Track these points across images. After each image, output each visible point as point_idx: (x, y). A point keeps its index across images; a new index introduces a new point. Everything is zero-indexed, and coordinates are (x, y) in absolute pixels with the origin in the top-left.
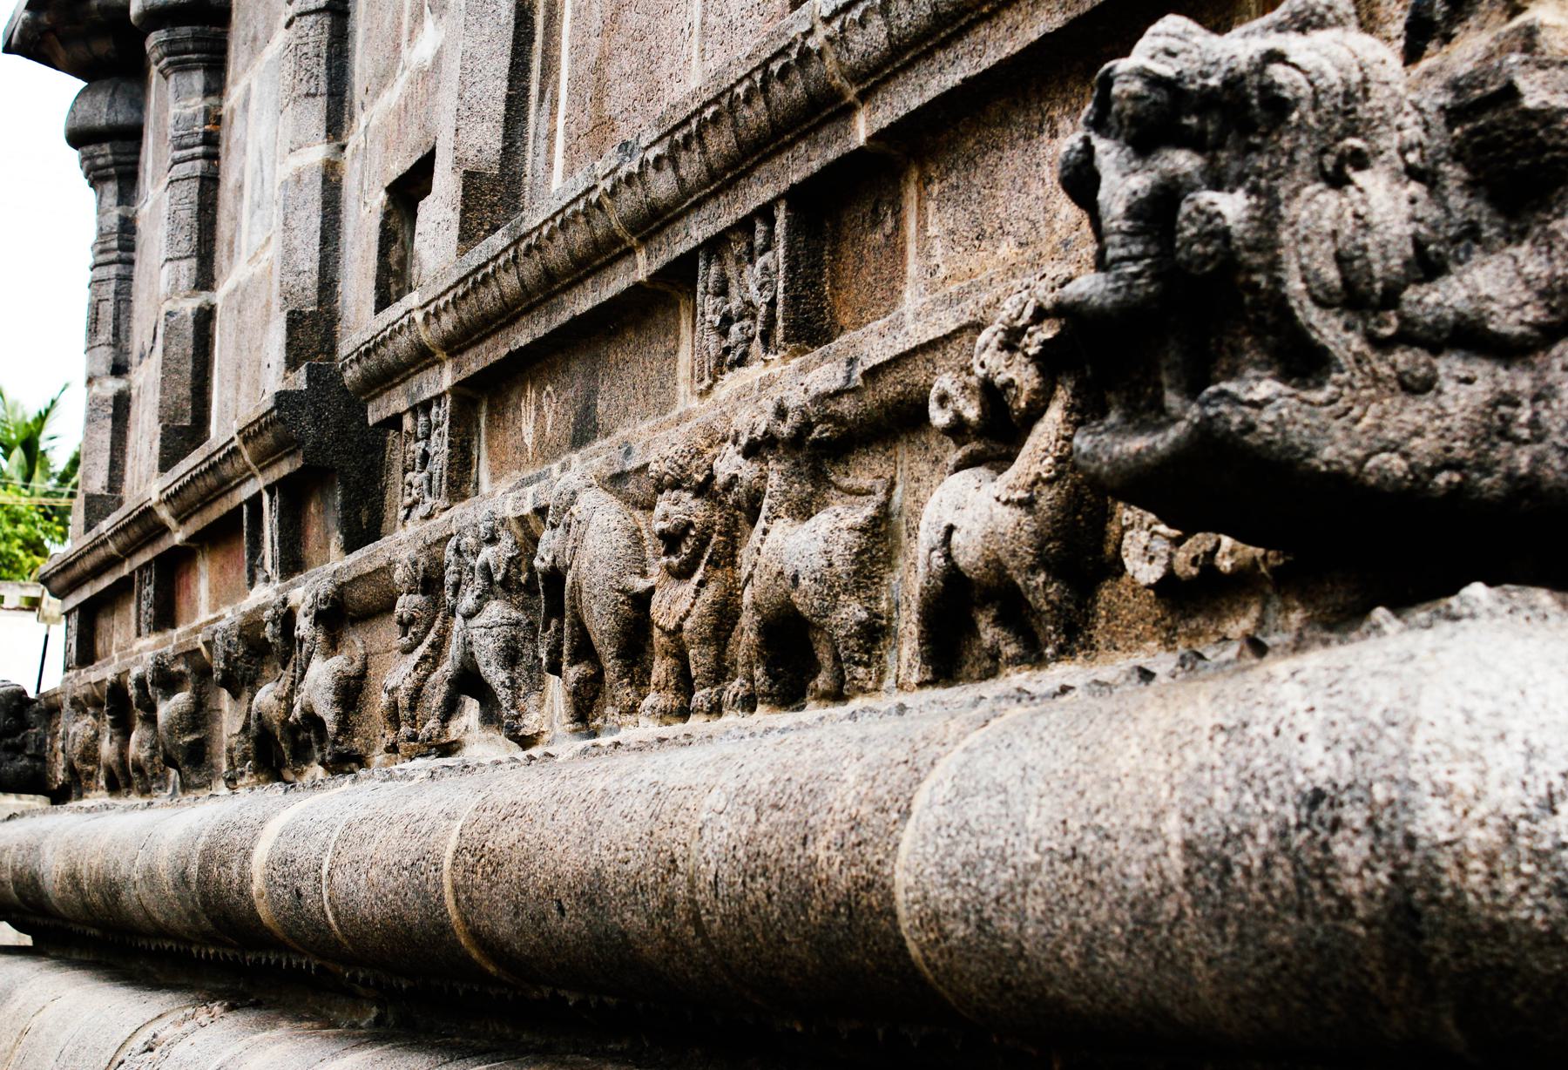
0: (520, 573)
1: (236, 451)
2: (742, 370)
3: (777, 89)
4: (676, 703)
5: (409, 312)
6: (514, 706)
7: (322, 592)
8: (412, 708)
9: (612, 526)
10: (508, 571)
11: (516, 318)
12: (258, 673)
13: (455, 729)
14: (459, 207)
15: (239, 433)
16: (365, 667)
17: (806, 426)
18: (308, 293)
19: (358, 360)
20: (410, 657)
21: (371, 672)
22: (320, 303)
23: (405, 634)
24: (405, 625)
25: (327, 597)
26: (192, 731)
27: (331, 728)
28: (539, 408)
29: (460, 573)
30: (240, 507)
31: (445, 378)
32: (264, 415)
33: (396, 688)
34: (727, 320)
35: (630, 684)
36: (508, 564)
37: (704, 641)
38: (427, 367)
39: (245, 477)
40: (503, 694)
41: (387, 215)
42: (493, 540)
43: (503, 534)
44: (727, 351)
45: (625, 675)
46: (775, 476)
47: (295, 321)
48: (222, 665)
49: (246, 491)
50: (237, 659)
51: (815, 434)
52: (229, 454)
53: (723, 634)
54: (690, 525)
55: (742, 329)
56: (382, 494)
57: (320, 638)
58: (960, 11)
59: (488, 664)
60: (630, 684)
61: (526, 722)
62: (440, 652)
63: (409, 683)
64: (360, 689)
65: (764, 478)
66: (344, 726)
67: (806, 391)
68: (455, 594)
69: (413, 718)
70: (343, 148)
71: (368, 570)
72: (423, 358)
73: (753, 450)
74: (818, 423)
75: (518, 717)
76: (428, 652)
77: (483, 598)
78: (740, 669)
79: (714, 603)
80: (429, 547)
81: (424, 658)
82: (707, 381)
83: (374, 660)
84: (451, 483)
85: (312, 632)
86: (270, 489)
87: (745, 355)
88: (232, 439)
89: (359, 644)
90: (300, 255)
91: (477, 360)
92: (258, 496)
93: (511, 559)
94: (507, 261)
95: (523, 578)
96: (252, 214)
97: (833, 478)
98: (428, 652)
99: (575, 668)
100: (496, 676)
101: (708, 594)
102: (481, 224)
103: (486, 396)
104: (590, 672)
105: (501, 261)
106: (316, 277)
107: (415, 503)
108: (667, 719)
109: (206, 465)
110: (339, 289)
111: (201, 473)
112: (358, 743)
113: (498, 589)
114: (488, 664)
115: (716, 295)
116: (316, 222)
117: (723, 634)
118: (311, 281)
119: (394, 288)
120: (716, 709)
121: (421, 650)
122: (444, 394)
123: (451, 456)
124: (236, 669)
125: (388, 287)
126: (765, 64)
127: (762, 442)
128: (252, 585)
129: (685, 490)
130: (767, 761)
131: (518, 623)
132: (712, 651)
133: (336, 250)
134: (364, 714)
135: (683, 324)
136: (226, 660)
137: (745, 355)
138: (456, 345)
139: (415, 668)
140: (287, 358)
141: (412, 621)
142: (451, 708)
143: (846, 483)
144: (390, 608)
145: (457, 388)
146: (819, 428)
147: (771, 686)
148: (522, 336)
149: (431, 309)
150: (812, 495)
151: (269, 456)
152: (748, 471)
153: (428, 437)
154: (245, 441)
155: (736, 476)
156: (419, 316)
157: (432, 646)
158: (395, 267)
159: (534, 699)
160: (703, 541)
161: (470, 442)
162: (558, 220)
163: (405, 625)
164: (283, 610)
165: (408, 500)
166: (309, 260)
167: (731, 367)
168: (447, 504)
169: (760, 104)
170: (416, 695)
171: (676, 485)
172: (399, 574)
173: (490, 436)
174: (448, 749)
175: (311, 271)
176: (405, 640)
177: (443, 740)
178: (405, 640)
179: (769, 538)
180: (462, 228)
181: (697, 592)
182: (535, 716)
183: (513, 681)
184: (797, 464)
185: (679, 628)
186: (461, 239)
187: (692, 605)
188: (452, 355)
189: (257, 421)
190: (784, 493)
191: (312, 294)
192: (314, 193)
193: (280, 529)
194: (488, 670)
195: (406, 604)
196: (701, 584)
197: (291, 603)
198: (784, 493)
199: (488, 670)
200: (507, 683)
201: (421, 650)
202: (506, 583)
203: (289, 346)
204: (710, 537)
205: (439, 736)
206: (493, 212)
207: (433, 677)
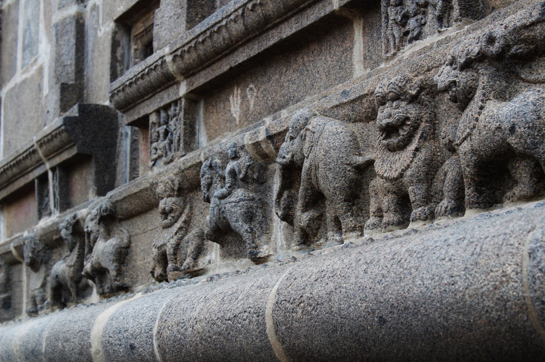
0: (254, 173)
1: (34, 152)
2: (418, 42)
3: (187, 56)
4: (396, 219)
5: (162, 57)
6: (253, 242)
7: (104, 206)
8: (175, 254)
9: (339, 131)
10: (247, 172)
11: (236, 49)
12: (50, 258)
13: (202, 262)
14: (186, 6)
15: (37, 142)
16: (130, 242)
17: (506, 47)
18: (70, 75)
19: (123, 90)
20: (170, 229)
21: (133, 245)
22: (76, 80)
23: (166, 218)
24: (165, 214)
25: (107, 208)
26: (5, 292)
27: (113, 273)
28: (244, 97)
29: (212, 178)
30: (33, 182)
31: (183, 89)
32: (55, 130)
33: (164, 245)
34: (406, 17)
35: (352, 215)
36: (247, 169)
37: (419, 181)
38: (171, 85)
39: (40, 163)
40: (246, 236)
41: (115, 33)
42: (235, 157)
43: (242, 153)
44: (406, 33)
45: (349, 211)
46: (483, 78)
47: (64, 88)
48: (30, 255)
49: (38, 172)
50: (39, 251)
51: (513, 50)
52: (30, 154)
53: (430, 177)
54: (408, 119)
55: (417, 20)
56: (115, 168)
57: (102, 230)
58: (297, 5)
59: (237, 221)
60: (352, 215)
61: (261, 250)
62: (189, 225)
63: (173, 241)
64: (127, 254)
65: (477, 80)
66: (120, 273)
67: (506, 27)
68: (208, 190)
69: (176, 259)
70: (85, 7)
71: (136, 191)
72: (167, 81)
73: (467, 65)
74: (514, 45)
75: (256, 247)
76: (183, 225)
77: (233, 187)
78: (446, 194)
79: (425, 159)
80: (183, 171)
81: (180, 228)
82: (393, 51)
83: (133, 240)
84: (186, 143)
85: (97, 228)
86: (53, 169)
87: (420, 34)
88: (33, 146)
89: (125, 231)
90: (65, 57)
91: (201, 79)
92: (45, 174)
93: (249, 166)
94: (237, 16)
95: (255, 176)
96: (24, 50)
97: (523, 76)
98: (183, 225)
99: (306, 214)
100: (242, 227)
101: (422, 155)
102: (197, 14)
103: (210, 94)
104: (316, 214)
105: (232, 17)
106: (73, 68)
107: (160, 157)
108: (390, 227)
109: (15, 162)
110: (85, 73)
111: (11, 167)
112: (127, 281)
113: (241, 183)
114: (237, 221)
115: (396, 6)
116: (73, 41)
117: (430, 177)
118: (71, 69)
119: (119, 68)
120: (431, 216)
121: (178, 225)
122: (180, 99)
123: (185, 129)
124: (38, 256)
125: (116, 67)
126: (245, 5)
127: (475, 60)
128: (40, 218)
129: (402, 101)
130: (369, 272)
131: (253, 199)
132: (425, 186)
133: (83, 55)
134: (130, 266)
135: (356, 33)
136: (33, 252)
137: (420, 34)
138: (188, 73)
139: (176, 234)
140: (61, 106)
141: (171, 210)
142: (199, 251)
143: (532, 78)
144: (157, 205)
145: (187, 96)
146: (515, 47)
147: (478, 198)
148: (241, 57)
149: (179, 53)
150: (506, 87)
151: (55, 151)
152: (463, 78)
153: (166, 123)
154: (41, 146)
155: (454, 82)
156: (169, 59)
157: (185, 222)
158: (119, 58)
159: (264, 238)
160: (415, 128)
161: (194, 122)
162: (208, 33)
163: (165, 214)
164: (74, 221)
165: (155, 156)
166: (69, 59)
167: (410, 41)
168: (183, 153)
169: (240, 21)
170: (177, 247)
171: (397, 98)
172: (160, 189)
173: (206, 118)
174: (195, 273)
175: (71, 65)
176: (166, 221)
177: (196, 269)
178: (166, 221)
179: (484, 112)
180: (187, 16)
181: (415, 155)
182: (265, 247)
183: (251, 229)
184: (497, 70)
185: (401, 175)
186: (188, 22)
187: (411, 162)
188: (186, 78)
189: (50, 134)
190: (491, 86)
191: (72, 76)
192: (72, 29)
193: (60, 188)
194: (237, 225)
195: (165, 203)
196: (417, 150)
197: (79, 216)
198: (491, 86)
199: (237, 225)
200: (249, 230)
201: (178, 225)
202: (245, 179)
203: (61, 100)
204: (419, 125)
205: (193, 266)
206: (203, 9)
207: (186, 238)
